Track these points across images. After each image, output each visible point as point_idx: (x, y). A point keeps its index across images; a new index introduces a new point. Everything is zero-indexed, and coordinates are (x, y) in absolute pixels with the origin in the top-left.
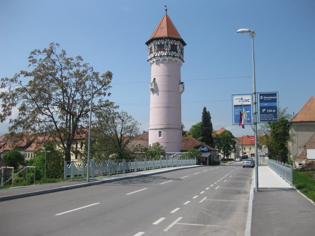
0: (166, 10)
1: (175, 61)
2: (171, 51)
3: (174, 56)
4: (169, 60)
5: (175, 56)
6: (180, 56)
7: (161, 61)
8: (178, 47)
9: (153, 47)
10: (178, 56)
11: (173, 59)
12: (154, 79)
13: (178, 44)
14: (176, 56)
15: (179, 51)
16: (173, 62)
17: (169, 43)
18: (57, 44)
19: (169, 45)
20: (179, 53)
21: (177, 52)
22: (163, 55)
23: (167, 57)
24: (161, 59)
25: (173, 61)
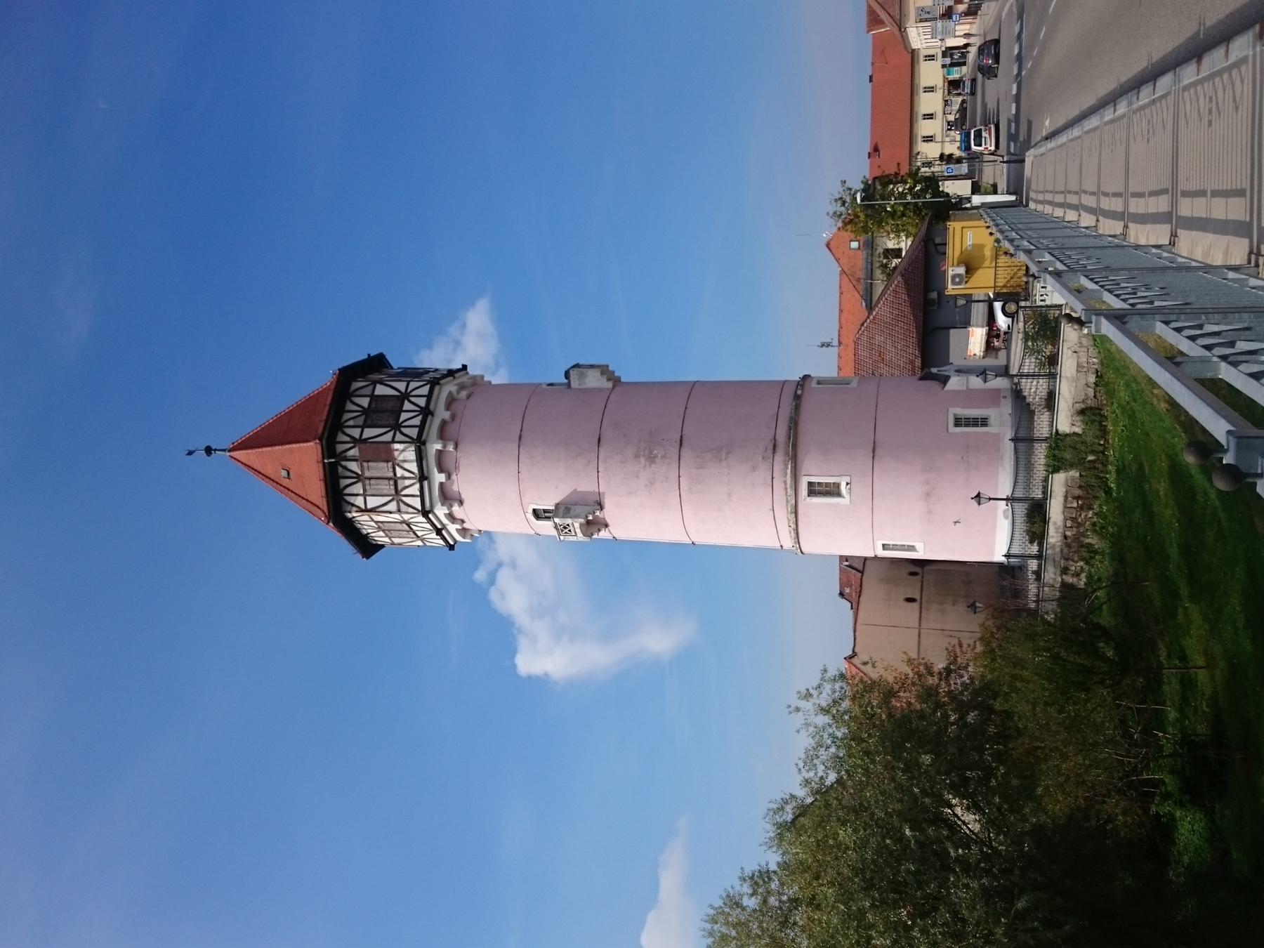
0: (209, 450)
1: (448, 407)
2: (397, 427)
3: (426, 412)
5: (423, 405)
8: (381, 390)
10: (425, 391)
11: (442, 413)
16: (453, 417)
17: (356, 433)
19: (369, 433)
21: (406, 396)
23: (424, 443)
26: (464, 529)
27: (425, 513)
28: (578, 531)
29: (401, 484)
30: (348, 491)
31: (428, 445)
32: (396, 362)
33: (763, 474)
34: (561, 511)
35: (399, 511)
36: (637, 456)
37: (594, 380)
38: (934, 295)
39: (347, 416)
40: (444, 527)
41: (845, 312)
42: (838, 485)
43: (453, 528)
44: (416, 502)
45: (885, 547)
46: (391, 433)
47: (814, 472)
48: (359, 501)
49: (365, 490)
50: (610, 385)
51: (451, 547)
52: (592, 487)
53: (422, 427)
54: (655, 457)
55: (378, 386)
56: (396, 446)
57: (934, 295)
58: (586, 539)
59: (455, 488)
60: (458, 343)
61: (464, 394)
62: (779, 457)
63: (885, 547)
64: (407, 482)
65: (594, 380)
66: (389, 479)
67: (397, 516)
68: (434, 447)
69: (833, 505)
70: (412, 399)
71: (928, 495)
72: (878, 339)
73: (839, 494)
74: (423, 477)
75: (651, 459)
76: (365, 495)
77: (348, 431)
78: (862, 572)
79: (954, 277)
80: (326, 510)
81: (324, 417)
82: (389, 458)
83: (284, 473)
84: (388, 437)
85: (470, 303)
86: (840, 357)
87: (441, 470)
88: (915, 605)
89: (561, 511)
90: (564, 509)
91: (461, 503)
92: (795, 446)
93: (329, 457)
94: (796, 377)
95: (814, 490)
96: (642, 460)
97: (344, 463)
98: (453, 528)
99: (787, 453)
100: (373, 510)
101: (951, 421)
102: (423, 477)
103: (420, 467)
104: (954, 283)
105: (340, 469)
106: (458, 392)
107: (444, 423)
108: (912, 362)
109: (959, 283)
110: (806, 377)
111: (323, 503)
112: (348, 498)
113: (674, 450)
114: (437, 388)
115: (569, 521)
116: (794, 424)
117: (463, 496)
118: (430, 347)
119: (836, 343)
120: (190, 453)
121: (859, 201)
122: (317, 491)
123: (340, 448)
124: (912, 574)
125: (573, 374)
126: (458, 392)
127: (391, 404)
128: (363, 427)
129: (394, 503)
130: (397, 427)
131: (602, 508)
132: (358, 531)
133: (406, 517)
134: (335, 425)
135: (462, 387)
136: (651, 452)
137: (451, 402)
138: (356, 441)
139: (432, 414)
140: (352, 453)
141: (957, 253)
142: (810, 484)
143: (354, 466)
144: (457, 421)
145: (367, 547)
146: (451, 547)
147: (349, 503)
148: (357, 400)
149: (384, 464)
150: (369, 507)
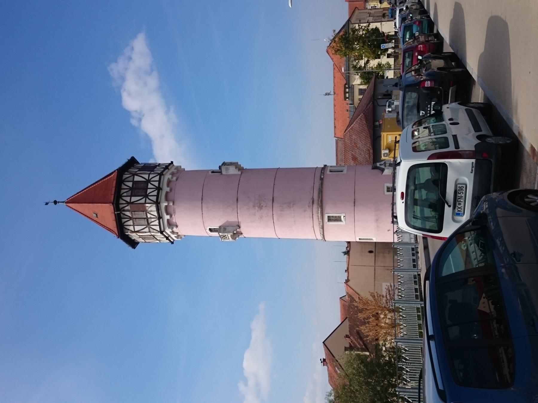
0: (55, 202)
1: (168, 186)
2: (146, 196)
3: (159, 189)
5: (157, 185)
8: (137, 178)
9: (139, 234)
10: (157, 178)
11: (166, 189)
12: (211, 230)
15: (146, 176)
16: (171, 190)
17: (128, 199)
19: (134, 199)
21: (148, 181)
23: (159, 203)
25: (168, 189)
26: (178, 235)
27: (161, 232)
28: (230, 237)
29: (150, 221)
30: (126, 224)
31: (161, 204)
32: (141, 160)
33: (308, 213)
34: (222, 229)
35: (150, 232)
36: (254, 206)
37: (232, 171)
38: (377, 123)
39: (123, 191)
40: (169, 236)
41: (336, 78)
42: (340, 217)
43: (173, 236)
44: (158, 228)
45: (360, 239)
46: (144, 199)
47: (330, 212)
48: (131, 228)
49: (133, 223)
50: (240, 173)
51: (172, 243)
52: (236, 220)
53: (158, 196)
54: (262, 206)
55: (135, 176)
56: (147, 205)
57: (377, 123)
58: (233, 240)
59: (174, 221)
60: (130, 58)
61: (175, 178)
62: (315, 206)
63: (360, 239)
64: (153, 220)
65: (232, 171)
66: (145, 219)
67: (149, 234)
68: (164, 204)
69: (338, 225)
70: (152, 183)
71: (377, 220)
72: (354, 137)
73: (341, 220)
74: (160, 217)
75: (260, 207)
76: (134, 225)
79: (384, 154)
80: (117, 232)
81: (113, 192)
82: (145, 210)
83: (95, 215)
84: (143, 201)
85: (134, 36)
86: (334, 100)
87: (167, 214)
88: (373, 254)
89: (222, 229)
90: (222, 229)
91: (177, 226)
92: (322, 201)
93: (117, 211)
95: (330, 219)
96: (257, 208)
97: (123, 212)
98: (173, 236)
99: (318, 204)
100: (138, 232)
101: (386, 189)
102: (160, 217)
103: (158, 213)
104: (384, 156)
105: (122, 215)
106: (172, 178)
107: (167, 193)
108: (369, 150)
109: (386, 156)
110: (325, 166)
111: (116, 230)
112: (126, 227)
113: (270, 203)
114: (162, 177)
115: (226, 234)
116: (321, 191)
117: (178, 224)
118: (116, 61)
119: (332, 93)
120: (47, 204)
121: (343, 71)
122: (112, 225)
123: (121, 206)
124: (371, 252)
125: (223, 168)
126: (172, 178)
127: (142, 185)
128: (131, 196)
130: (146, 196)
131: (240, 227)
132: (130, 238)
133: (153, 234)
134: (118, 196)
135: (173, 174)
136: (260, 204)
137: (169, 182)
138: (128, 203)
139: (162, 189)
140: (127, 208)
141: (385, 144)
142: (328, 217)
143: (128, 213)
144: (173, 191)
145: (133, 244)
146: (172, 243)
147: (127, 229)
148: (127, 183)
149: (142, 213)
150: (136, 230)
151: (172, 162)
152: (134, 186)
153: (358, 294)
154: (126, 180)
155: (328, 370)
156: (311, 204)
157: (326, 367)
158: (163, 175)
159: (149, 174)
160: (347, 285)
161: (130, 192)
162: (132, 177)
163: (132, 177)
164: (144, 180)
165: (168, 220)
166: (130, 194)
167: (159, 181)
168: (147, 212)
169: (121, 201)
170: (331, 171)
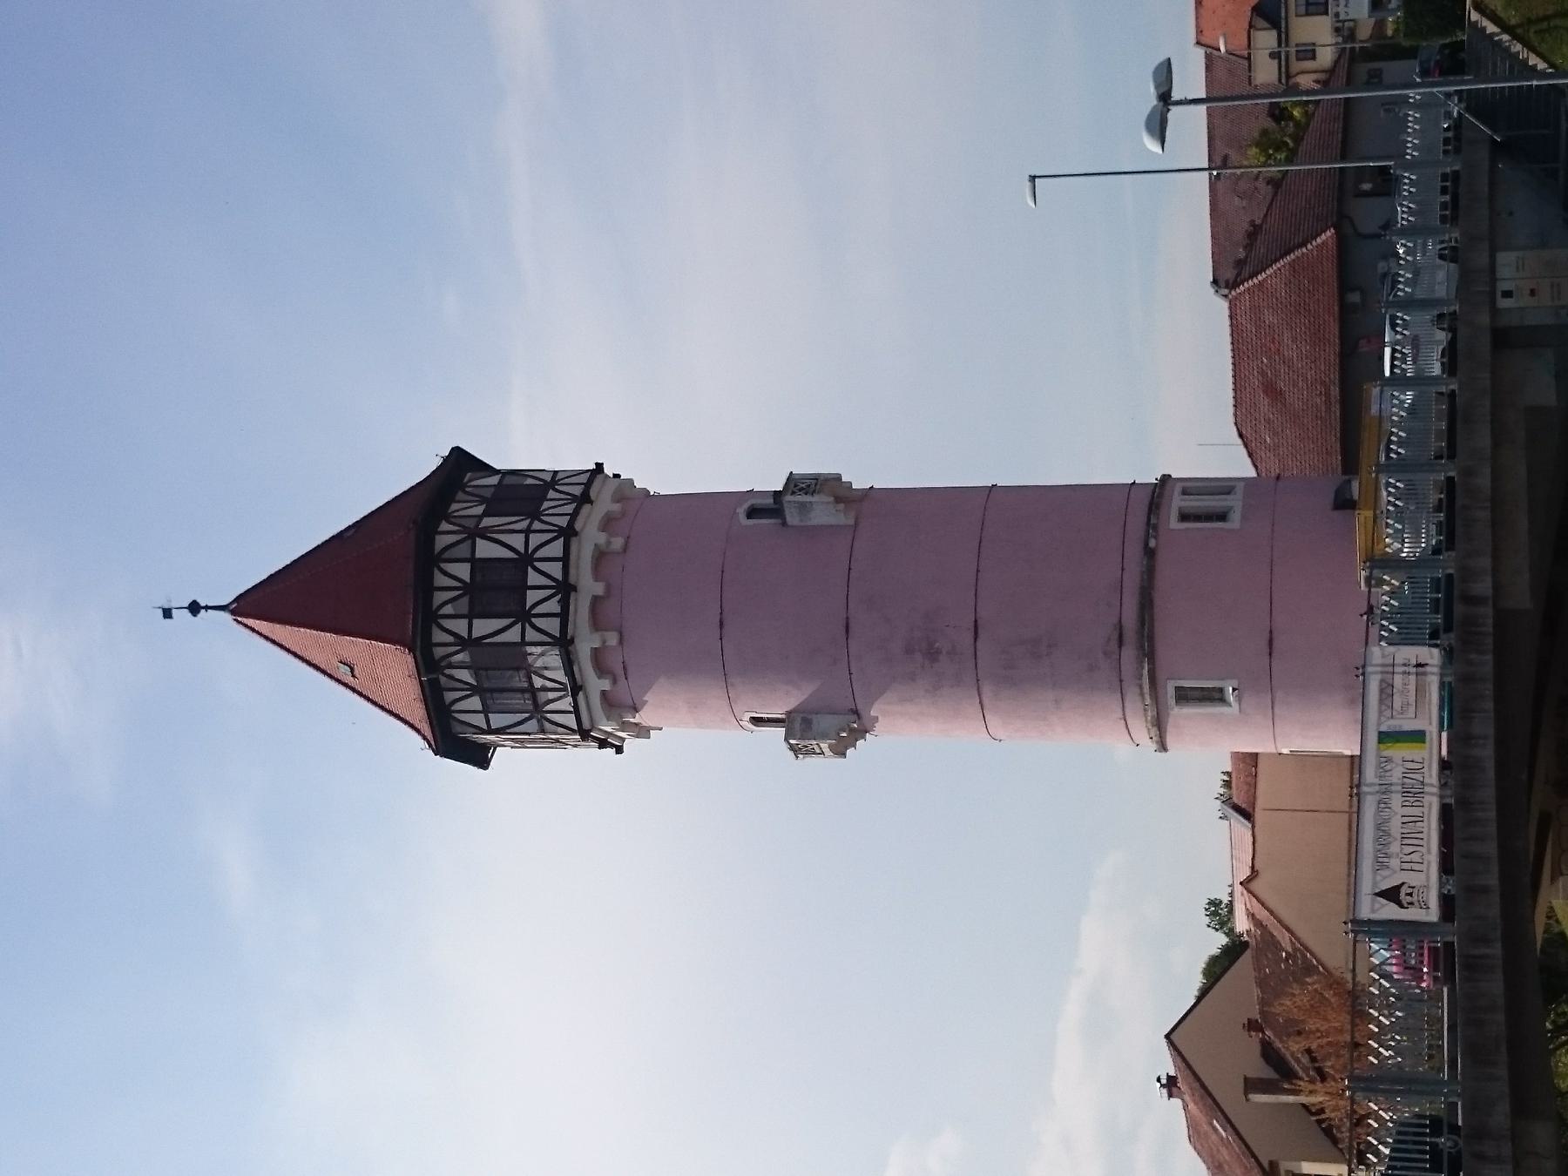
0: (194, 608)
1: (597, 577)
2: (524, 616)
3: (565, 589)
4: (601, 670)
5: (559, 575)
6: (574, 498)
7: (615, 681)
8: (485, 549)
10: (556, 549)
11: (588, 586)
13: (463, 550)
14: (563, 522)
15: (517, 541)
16: (608, 588)
17: (460, 627)
18: (1159, 1080)
19: (482, 627)
20: (535, 540)
21: (526, 560)
22: (555, 569)
23: (572, 641)
24: (596, 685)
25: (599, 589)
29: (543, 697)
30: (457, 707)
35: (543, 731)
41: (1218, 142)
42: (1221, 690)
48: (479, 720)
54: (938, 652)
56: (530, 649)
64: (551, 695)
65: (823, 513)
66: (523, 691)
72: (1269, 317)
77: (447, 624)
78: (1249, 58)
94: (1151, 478)
95: (1184, 696)
102: (576, 689)
103: (570, 672)
110: (1166, 478)
111: (418, 713)
123: (439, 652)
128: (470, 617)
129: (534, 721)
130: (524, 616)
137: (600, 556)
139: (574, 589)
142: (1178, 689)
148: (452, 568)
151: (599, 466)
152: (478, 578)
153: (1288, 929)
154: (446, 555)
155: (1185, 1107)
156: (1114, 645)
157: (1177, 1102)
158: (576, 534)
159: (527, 532)
160: (1249, 891)
161: (466, 600)
162: (466, 546)
163: (466, 546)
164: (511, 555)
165: (604, 693)
166: (465, 611)
167: (565, 560)
168: (529, 672)
169: (438, 636)
170: (1184, 517)
